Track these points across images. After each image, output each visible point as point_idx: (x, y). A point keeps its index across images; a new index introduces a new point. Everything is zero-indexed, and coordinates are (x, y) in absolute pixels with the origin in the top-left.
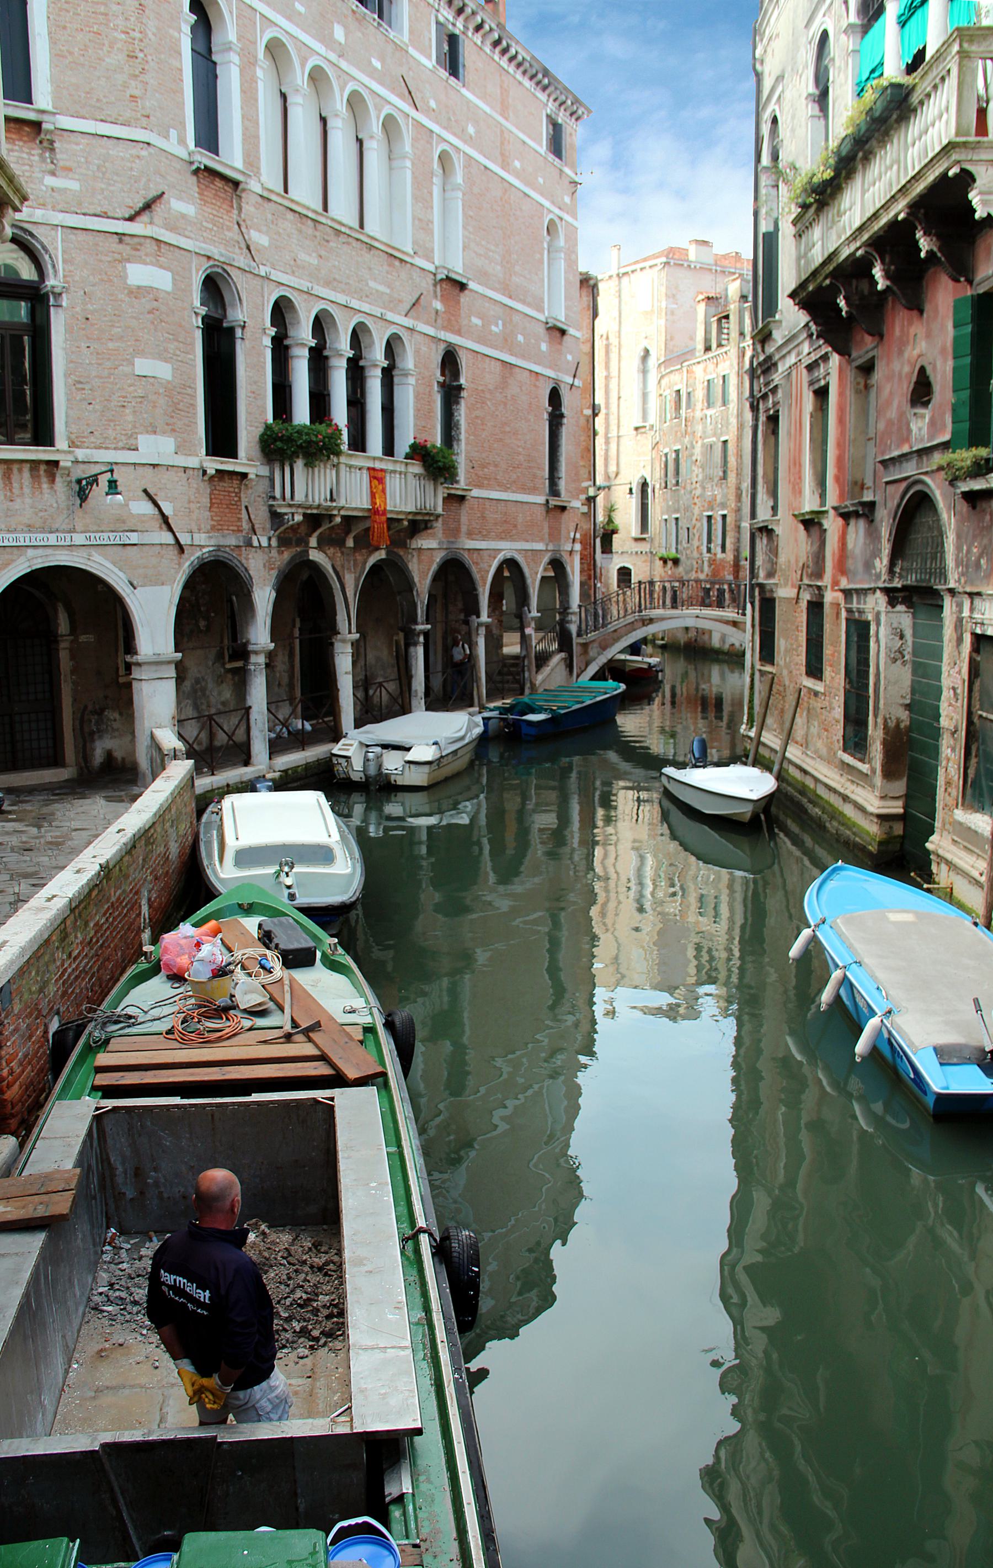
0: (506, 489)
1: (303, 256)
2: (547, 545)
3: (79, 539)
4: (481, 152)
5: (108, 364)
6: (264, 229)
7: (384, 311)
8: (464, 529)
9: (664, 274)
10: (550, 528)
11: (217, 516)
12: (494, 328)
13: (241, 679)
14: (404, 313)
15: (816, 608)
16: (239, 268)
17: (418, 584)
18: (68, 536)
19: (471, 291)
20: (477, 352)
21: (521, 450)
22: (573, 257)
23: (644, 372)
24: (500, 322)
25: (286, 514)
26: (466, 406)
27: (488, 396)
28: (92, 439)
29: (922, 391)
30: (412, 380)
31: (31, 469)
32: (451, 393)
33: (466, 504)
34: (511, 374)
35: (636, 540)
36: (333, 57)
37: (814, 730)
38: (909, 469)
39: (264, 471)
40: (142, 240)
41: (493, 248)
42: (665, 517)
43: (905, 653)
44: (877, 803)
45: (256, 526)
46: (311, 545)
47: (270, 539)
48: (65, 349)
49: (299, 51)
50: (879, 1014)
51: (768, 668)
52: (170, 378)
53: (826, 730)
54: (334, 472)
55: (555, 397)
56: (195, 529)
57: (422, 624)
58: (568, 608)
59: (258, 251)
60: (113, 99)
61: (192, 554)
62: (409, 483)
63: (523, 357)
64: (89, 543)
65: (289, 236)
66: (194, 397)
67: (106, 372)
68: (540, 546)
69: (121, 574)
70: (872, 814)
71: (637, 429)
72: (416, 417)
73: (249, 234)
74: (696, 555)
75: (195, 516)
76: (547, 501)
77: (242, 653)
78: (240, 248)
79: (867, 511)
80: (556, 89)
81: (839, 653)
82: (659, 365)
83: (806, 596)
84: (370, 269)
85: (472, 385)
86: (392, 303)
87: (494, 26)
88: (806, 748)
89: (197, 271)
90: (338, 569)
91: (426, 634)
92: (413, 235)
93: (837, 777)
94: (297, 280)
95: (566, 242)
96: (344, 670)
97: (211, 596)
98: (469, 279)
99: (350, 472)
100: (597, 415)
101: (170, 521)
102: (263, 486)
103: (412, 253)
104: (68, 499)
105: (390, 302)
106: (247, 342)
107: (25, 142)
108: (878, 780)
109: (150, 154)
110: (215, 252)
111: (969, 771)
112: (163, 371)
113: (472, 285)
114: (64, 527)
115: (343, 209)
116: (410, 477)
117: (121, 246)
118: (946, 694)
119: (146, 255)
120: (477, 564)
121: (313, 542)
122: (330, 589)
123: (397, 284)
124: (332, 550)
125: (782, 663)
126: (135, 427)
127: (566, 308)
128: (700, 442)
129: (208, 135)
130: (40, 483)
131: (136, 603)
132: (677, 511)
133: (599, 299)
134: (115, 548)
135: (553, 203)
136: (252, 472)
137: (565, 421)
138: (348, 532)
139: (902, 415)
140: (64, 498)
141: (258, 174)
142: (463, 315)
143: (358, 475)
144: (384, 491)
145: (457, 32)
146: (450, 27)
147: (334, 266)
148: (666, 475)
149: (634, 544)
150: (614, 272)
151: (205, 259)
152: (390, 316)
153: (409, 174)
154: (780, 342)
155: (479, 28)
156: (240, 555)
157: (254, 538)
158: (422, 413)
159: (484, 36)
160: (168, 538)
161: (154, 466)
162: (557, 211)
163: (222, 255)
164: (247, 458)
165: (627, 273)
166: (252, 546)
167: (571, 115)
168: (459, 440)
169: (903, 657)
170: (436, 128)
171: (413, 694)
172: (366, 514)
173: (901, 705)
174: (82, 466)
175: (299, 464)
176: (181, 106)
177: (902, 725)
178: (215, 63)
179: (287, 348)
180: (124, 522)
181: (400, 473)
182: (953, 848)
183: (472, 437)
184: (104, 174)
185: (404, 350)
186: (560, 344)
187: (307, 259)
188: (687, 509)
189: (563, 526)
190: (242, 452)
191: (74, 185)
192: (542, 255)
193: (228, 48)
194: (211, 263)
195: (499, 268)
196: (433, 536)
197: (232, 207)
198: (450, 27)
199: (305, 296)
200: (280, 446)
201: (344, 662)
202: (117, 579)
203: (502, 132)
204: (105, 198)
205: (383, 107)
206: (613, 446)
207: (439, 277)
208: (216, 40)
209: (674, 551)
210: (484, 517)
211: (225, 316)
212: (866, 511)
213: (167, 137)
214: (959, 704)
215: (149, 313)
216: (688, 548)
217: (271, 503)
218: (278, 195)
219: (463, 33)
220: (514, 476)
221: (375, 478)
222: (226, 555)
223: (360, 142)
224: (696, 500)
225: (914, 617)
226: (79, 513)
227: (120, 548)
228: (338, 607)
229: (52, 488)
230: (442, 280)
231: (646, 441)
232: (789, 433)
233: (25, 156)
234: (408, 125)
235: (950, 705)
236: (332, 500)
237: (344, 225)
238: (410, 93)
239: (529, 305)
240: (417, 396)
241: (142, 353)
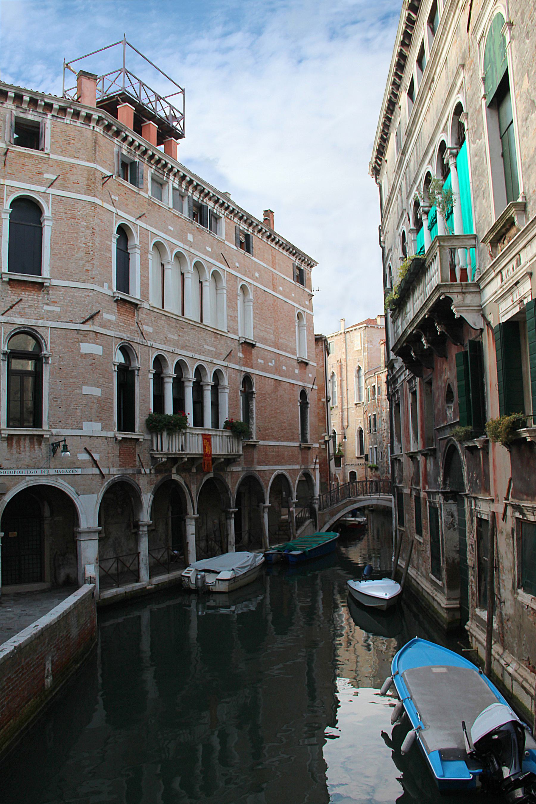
0: (278, 440)
1: (170, 336)
2: (301, 466)
3: (52, 472)
4: (262, 284)
5: (70, 389)
6: (151, 324)
7: (212, 359)
8: (255, 460)
9: (365, 332)
10: (302, 458)
11: (123, 459)
12: (270, 364)
13: (136, 537)
15: (418, 498)
16: (137, 343)
17: (231, 489)
18: (47, 470)
19: (258, 347)
22: (311, 329)
23: (359, 377)
24: (273, 361)
25: (159, 458)
26: (256, 402)
27: (268, 396)
28: (60, 424)
29: (449, 397)
30: (227, 391)
31: (30, 439)
32: (248, 396)
34: (280, 385)
35: (358, 458)
36: (187, 247)
37: (420, 562)
38: (447, 434)
39: (148, 437)
40: (88, 332)
41: (269, 327)
42: (371, 447)
43: (455, 524)
44: (445, 602)
45: (144, 464)
46: (173, 472)
47: (150, 470)
48: (49, 383)
49: (170, 246)
50: (415, 728)
51: (402, 529)
52: (100, 395)
53: (425, 562)
54: (183, 437)
55: (303, 394)
56: (111, 465)
58: (314, 496)
59: (147, 335)
60: (78, 271)
61: (109, 479)
62: (224, 440)
63: (286, 377)
64: (56, 474)
65: (163, 327)
66: (112, 403)
67: (68, 393)
68: (298, 467)
69: (72, 489)
70: (443, 608)
71: (356, 404)
73: (142, 327)
74: (385, 465)
75: (111, 460)
76: (300, 445)
77: (137, 526)
78: (138, 334)
79: (433, 452)
80: (299, 254)
81: (427, 522)
82: (366, 374)
83: (414, 493)
84: (205, 340)
86: (217, 355)
87: (267, 230)
88: (418, 570)
89: (116, 345)
90: (187, 483)
91: (235, 513)
92: (227, 323)
93: (430, 587)
94: (166, 347)
95: (307, 322)
96: (191, 533)
97: (119, 498)
98: (256, 342)
99: (192, 436)
100: (329, 401)
101: (98, 463)
102: (147, 445)
103: (227, 332)
104: (47, 453)
105: (216, 354)
106: (140, 377)
107: (36, 291)
108: (446, 590)
109: (94, 294)
110: (124, 336)
111: (481, 588)
112: (97, 392)
113: (258, 344)
114: (45, 466)
115: (192, 314)
116: (224, 437)
117: (78, 335)
118: (469, 548)
119: (90, 339)
120: (263, 477)
121: (174, 470)
122: (184, 493)
123: (219, 346)
124: (184, 474)
125: (407, 526)
126: (81, 418)
127: (308, 352)
128: (385, 410)
129: (124, 283)
130: (34, 446)
131: (79, 503)
132: (376, 444)
134: (69, 476)
135: (300, 305)
136: (141, 438)
137: (309, 406)
138: (193, 465)
139: (443, 406)
140: (45, 452)
141: (147, 300)
142: (253, 358)
143: (197, 438)
144: (210, 445)
145: (249, 233)
146: (246, 231)
147: (186, 340)
148: (370, 427)
149: (357, 460)
150: (342, 331)
151: (120, 340)
152: (215, 361)
153: (225, 296)
154: (398, 369)
155: (260, 231)
156: (135, 478)
157: (143, 470)
158: (233, 406)
159: (263, 234)
160: (96, 471)
161: (90, 437)
162: (302, 308)
163: (128, 337)
164: (139, 432)
165: (348, 332)
166: (141, 473)
167: (308, 265)
168: (253, 418)
169: (454, 526)
170: (239, 275)
171: (229, 543)
172: (201, 456)
173: (455, 551)
174: (55, 437)
175: (165, 434)
176: (110, 273)
177: (456, 561)
178: (129, 254)
179: (163, 378)
180: (74, 463)
181: (219, 436)
182: (476, 629)
184: (72, 304)
185: (223, 377)
186: (305, 369)
187: (172, 337)
188: (381, 443)
189: (309, 456)
190: (137, 429)
191: (58, 309)
192: (295, 329)
193: (135, 247)
194: (123, 341)
195: (272, 336)
196: (239, 465)
197: (134, 315)
198: (246, 231)
199: (171, 354)
200: (158, 424)
201: (191, 529)
202: (70, 491)
203: (273, 275)
204: (72, 314)
205: (212, 267)
206: (345, 413)
207: (241, 342)
208: (130, 243)
209: (375, 463)
210: (266, 454)
211: (130, 365)
212: (432, 453)
213: (103, 286)
214: (474, 553)
215: (90, 365)
216: (382, 462)
217: (151, 452)
218: (160, 310)
219: (252, 234)
220: (283, 434)
221: (205, 439)
222: (127, 478)
223: (201, 283)
224: (384, 438)
225: (458, 506)
226: (53, 459)
227: (72, 476)
228: (188, 502)
229: (40, 448)
230: (242, 343)
231: (361, 411)
232: (404, 413)
233: (36, 297)
234: (224, 274)
235: (471, 553)
236: (182, 450)
237: (191, 321)
238: (225, 260)
239: (288, 352)
240: (229, 398)
241: (87, 384)
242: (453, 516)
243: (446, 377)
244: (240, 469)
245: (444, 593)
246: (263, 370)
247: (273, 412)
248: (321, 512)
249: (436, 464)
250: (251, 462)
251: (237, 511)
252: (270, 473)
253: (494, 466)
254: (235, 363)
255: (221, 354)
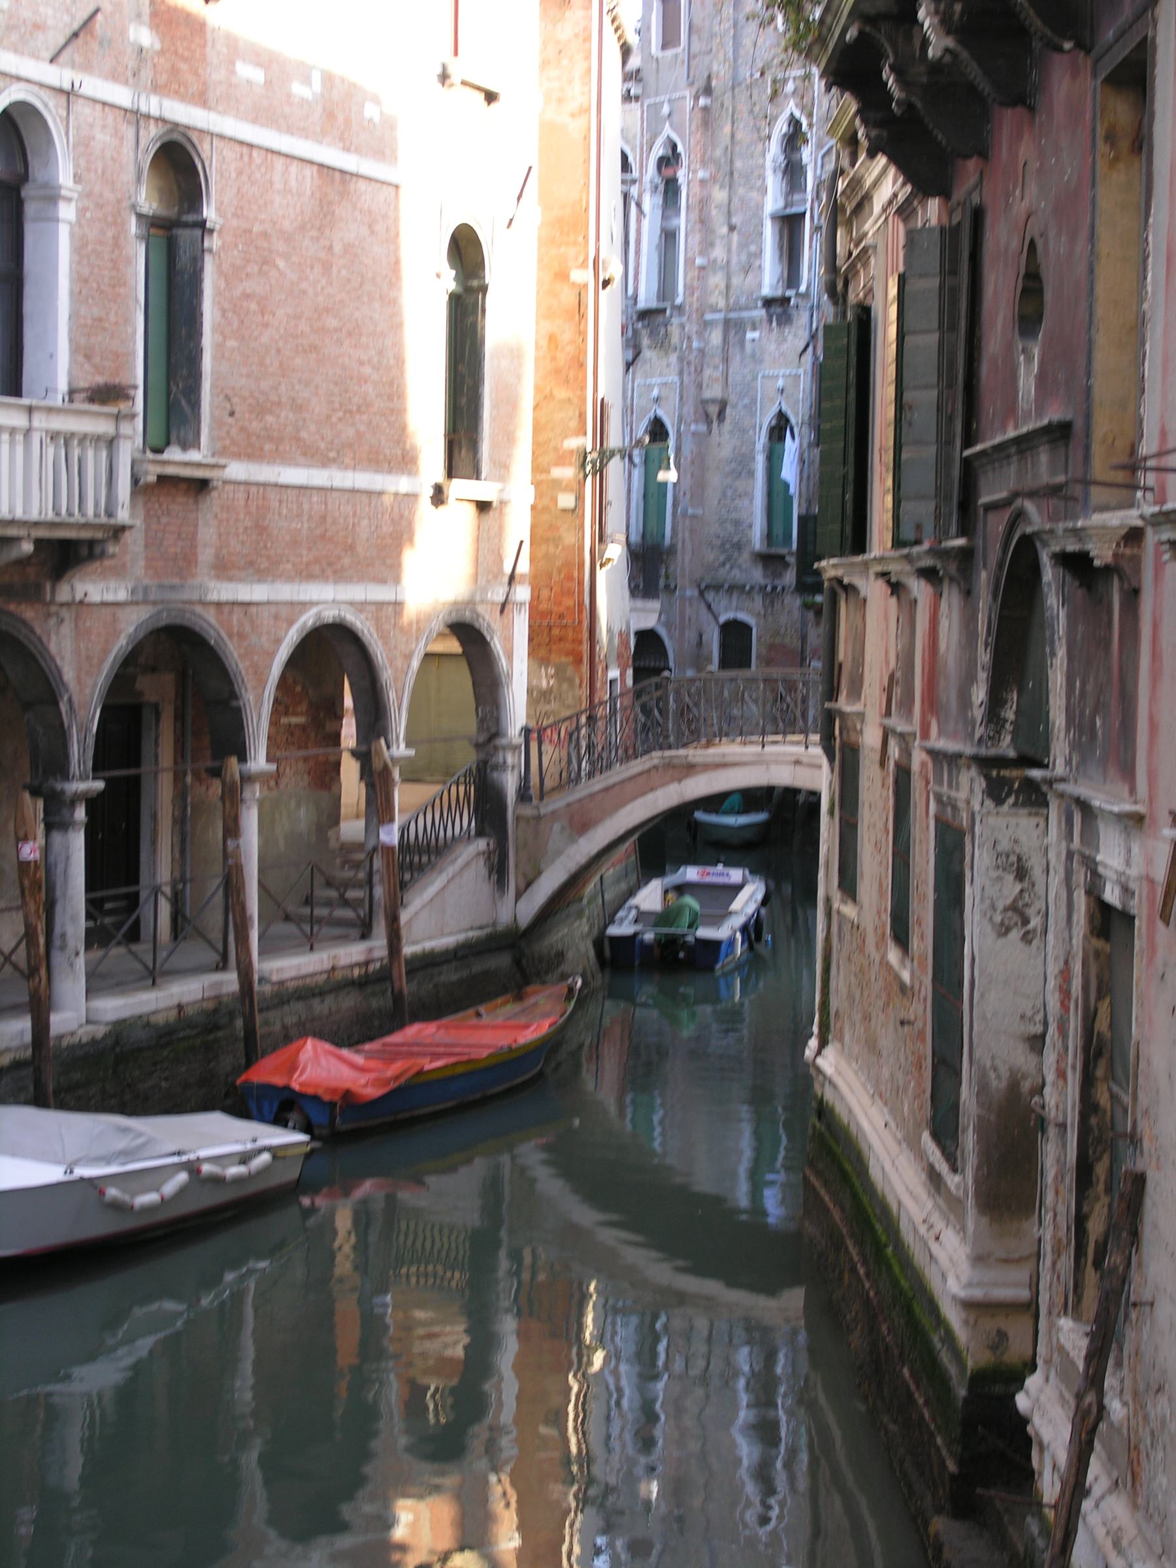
0: (325, 462)
8: (206, 555)
14: (48, 55)
15: (903, 776)
20: (251, 146)
21: (367, 370)
27: (280, 246)
33: (213, 502)
43: (1031, 912)
51: (849, 910)
57: (83, 778)
72: (76, 297)
85: (234, 222)
133: (639, 15)
169: (1026, 921)
171: (57, 942)
181: (13, 431)
183: (232, 343)
196: (120, 572)
210: (261, 529)
212: (953, 568)
220: (350, 432)
240: (79, 247)
242: (1021, 873)
243: (1025, 204)
244: (122, 596)
245: (963, 1229)
246: (263, 115)
247: (304, 326)
248: (527, 811)
249: (969, 621)
250: (185, 562)
251: (101, 794)
252: (276, 617)
253: (1155, 655)
254: (114, 76)
255: (38, 27)
